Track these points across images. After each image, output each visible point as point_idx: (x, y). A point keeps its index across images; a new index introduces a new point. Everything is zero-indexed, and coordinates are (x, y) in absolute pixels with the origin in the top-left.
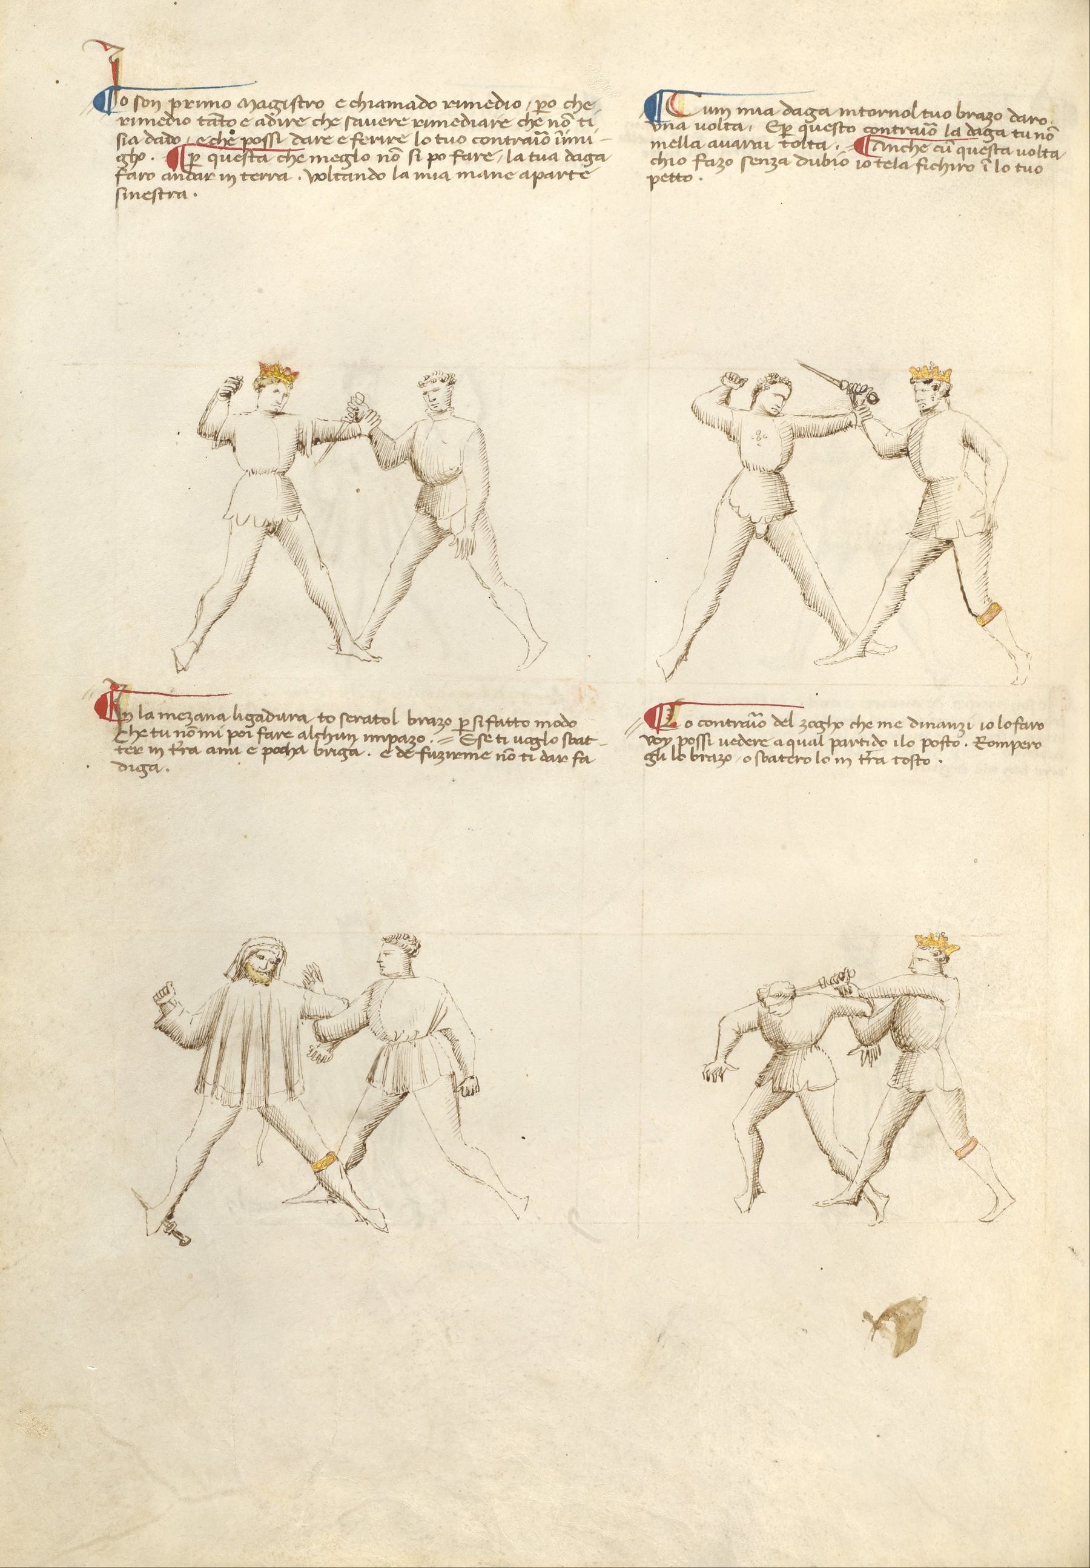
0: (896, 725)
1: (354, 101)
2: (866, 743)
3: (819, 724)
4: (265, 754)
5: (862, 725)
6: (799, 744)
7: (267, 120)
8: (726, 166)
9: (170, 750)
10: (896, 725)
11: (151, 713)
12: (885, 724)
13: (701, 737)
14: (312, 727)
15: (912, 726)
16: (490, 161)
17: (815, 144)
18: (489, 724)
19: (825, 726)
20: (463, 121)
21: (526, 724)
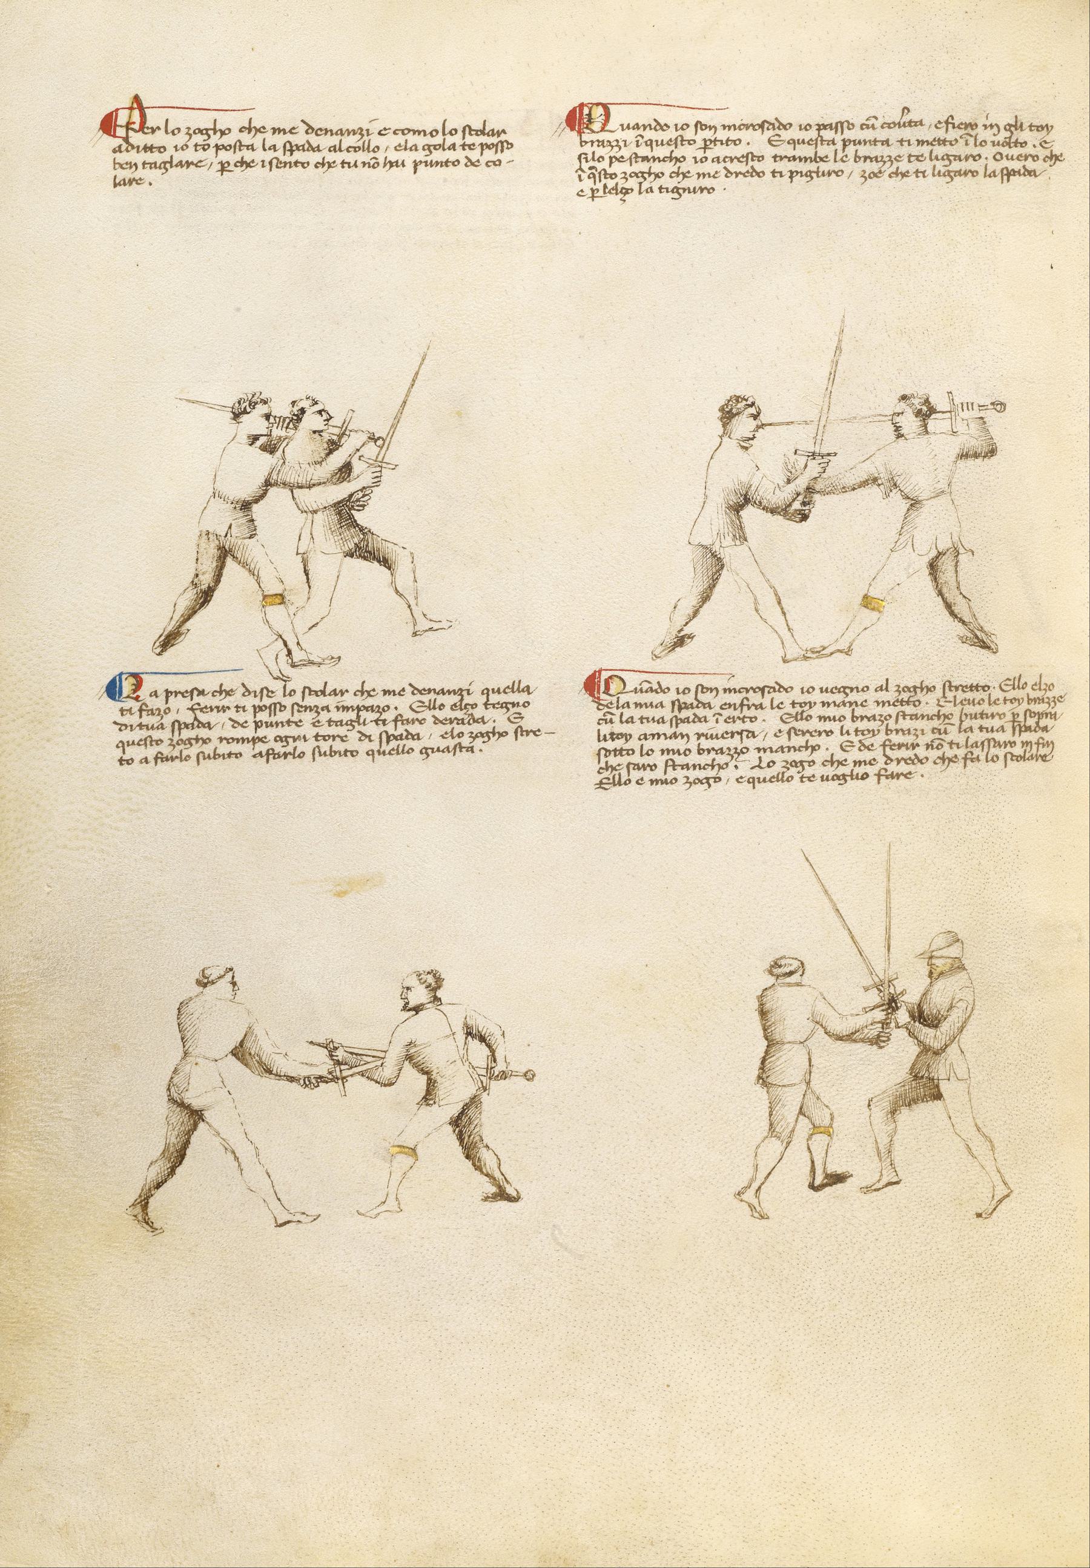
0: (862, 705)
1: (238, 162)
2: (779, 174)
3: (204, 132)
4: (791, 177)
5: (253, 131)
6: (759, 782)
7: (196, 723)
8: (629, 178)
9: (242, 158)
10: (862, 705)
11: (415, 145)
12: (860, 762)
13: (839, 125)
14: (990, 694)
15: (233, 727)
16: (845, 765)
17: (156, 148)
18: (879, 780)
19: (646, 175)
20: (752, 173)
21: (851, 127)
